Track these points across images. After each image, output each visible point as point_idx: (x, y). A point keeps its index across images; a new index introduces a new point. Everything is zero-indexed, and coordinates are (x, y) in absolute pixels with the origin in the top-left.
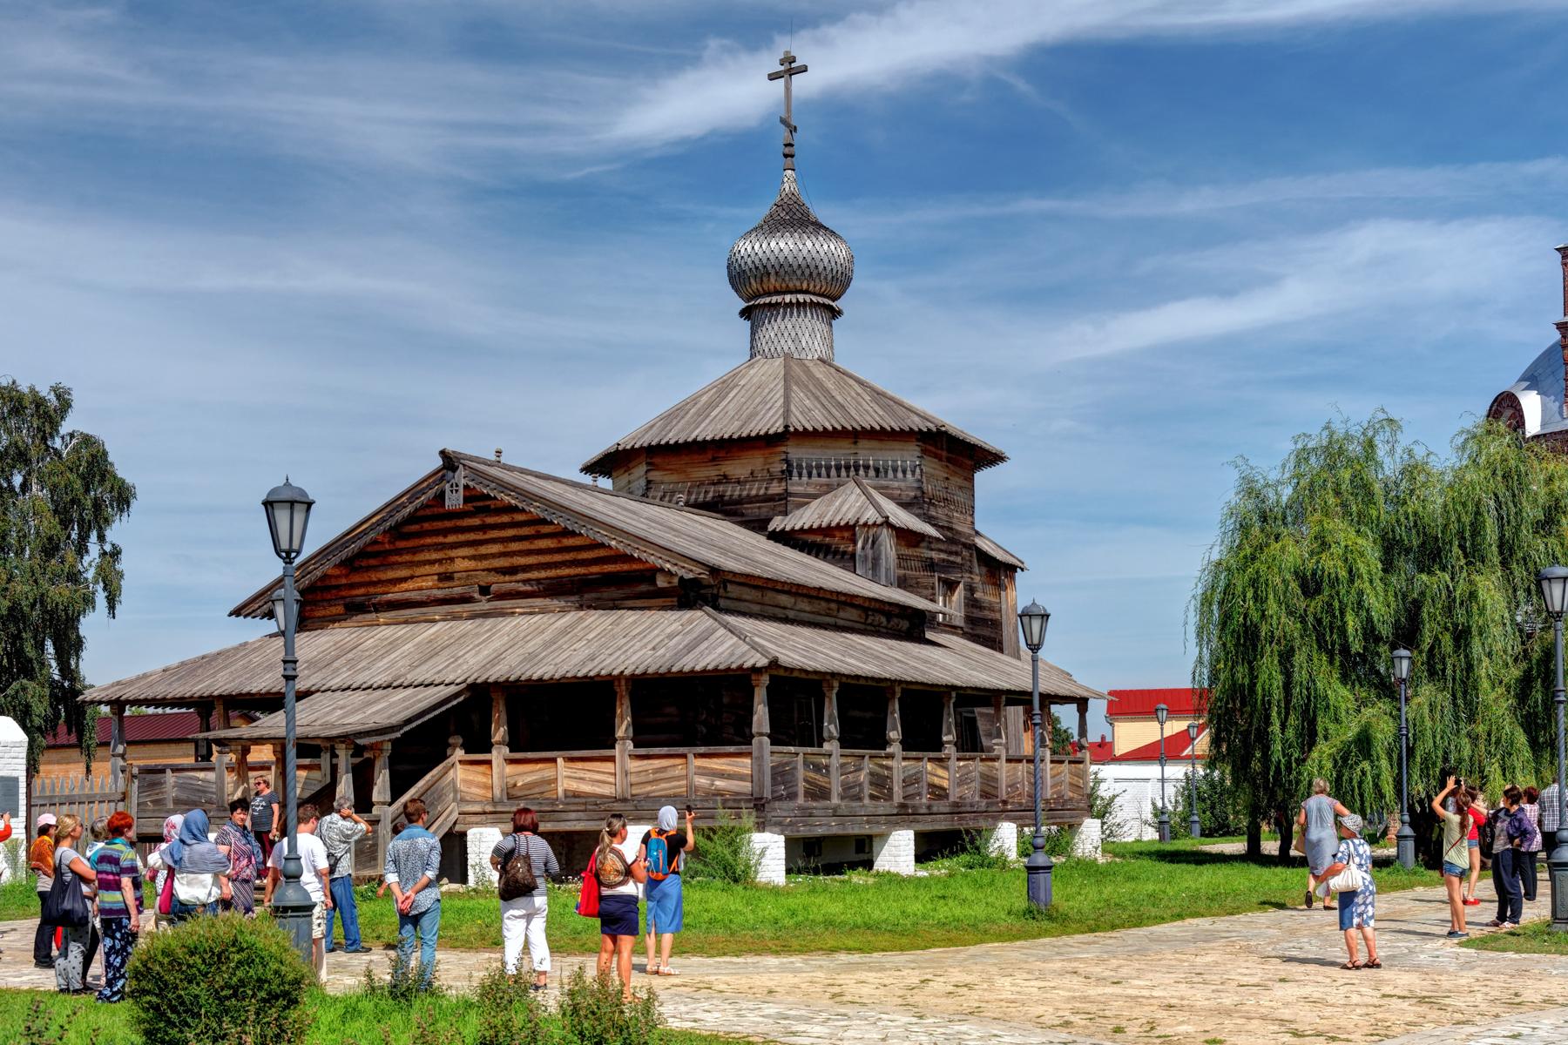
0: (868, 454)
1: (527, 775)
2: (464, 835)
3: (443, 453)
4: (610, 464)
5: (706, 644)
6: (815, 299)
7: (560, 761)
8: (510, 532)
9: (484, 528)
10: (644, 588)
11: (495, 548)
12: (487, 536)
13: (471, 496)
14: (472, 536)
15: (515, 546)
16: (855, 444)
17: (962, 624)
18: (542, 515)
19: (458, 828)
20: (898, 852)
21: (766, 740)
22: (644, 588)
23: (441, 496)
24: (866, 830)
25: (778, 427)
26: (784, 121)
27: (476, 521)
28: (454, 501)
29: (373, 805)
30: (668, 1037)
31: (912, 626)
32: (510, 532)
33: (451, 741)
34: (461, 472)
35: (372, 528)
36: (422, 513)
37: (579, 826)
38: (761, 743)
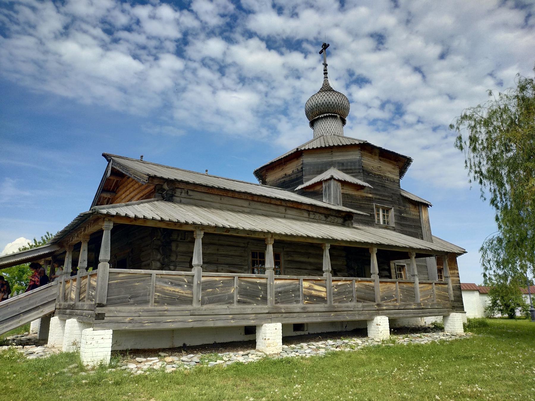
0: (339, 157)
4: (262, 174)
17: (394, 226)
20: (380, 328)
24: (252, 323)
26: (323, 64)
31: (345, 219)
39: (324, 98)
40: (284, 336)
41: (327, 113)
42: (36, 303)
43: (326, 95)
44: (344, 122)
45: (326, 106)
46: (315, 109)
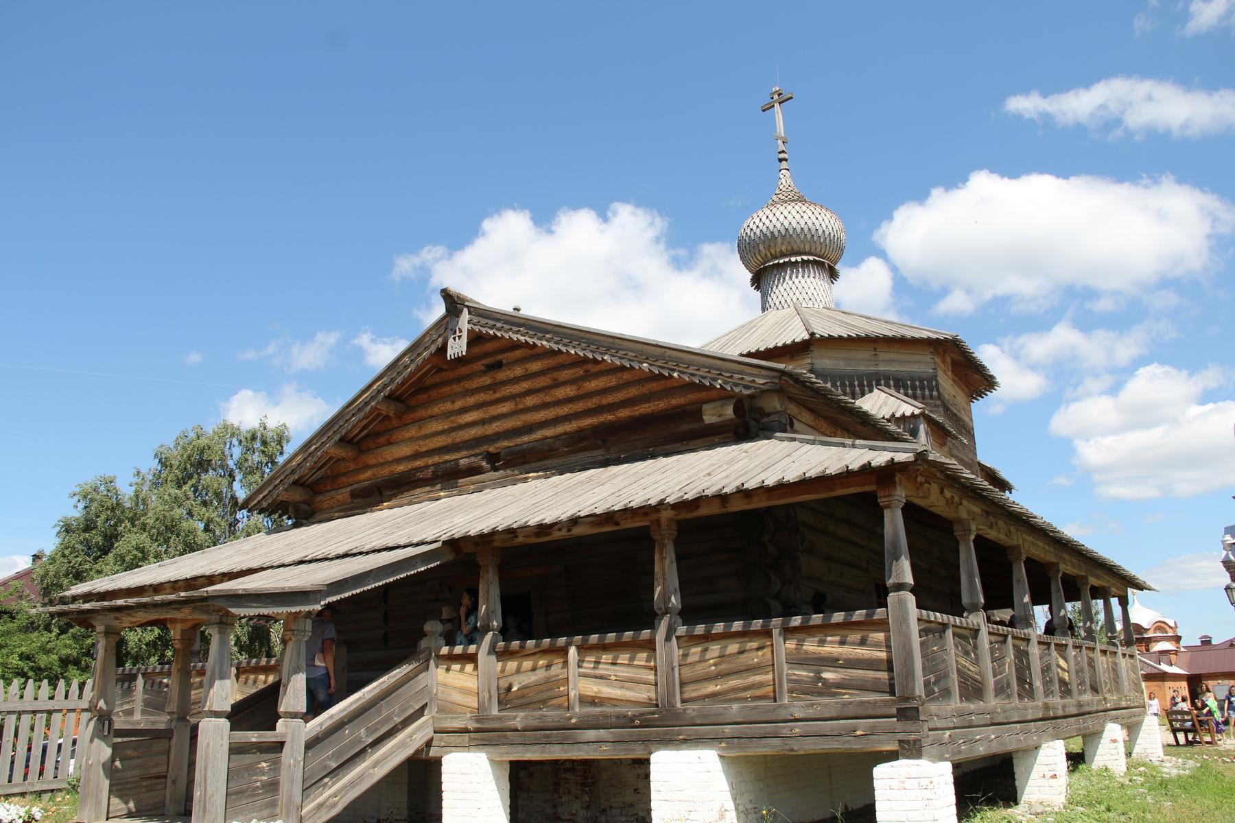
0: (891, 363)
1: (525, 673)
2: (438, 762)
3: (447, 295)
5: (790, 459)
6: (805, 258)
7: (573, 651)
8: (525, 385)
9: (493, 387)
10: (685, 427)
11: (505, 408)
12: (498, 395)
13: (475, 339)
14: (483, 397)
15: (530, 401)
16: (879, 354)
18: (555, 347)
19: (433, 752)
21: (911, 599)
22: (685, 427)
23: (443, 349)
25: (801, 335)
27: (487, 380)
28: (457, 347)
29: (278, 717)
30: (497, 206)
32: (525, 385)
33: (427, 627)
34: (465, 316)
35: (372, 398)
36: (429, 381)
37: (603, 752)
38: (902, 603)
39: (806, 217)
40: (640, 771)
41: (805, 254)
42: (388, 719)
43: (810, 213)
44: (833, 274)
45: (809, 236)
46: (779, 240)
